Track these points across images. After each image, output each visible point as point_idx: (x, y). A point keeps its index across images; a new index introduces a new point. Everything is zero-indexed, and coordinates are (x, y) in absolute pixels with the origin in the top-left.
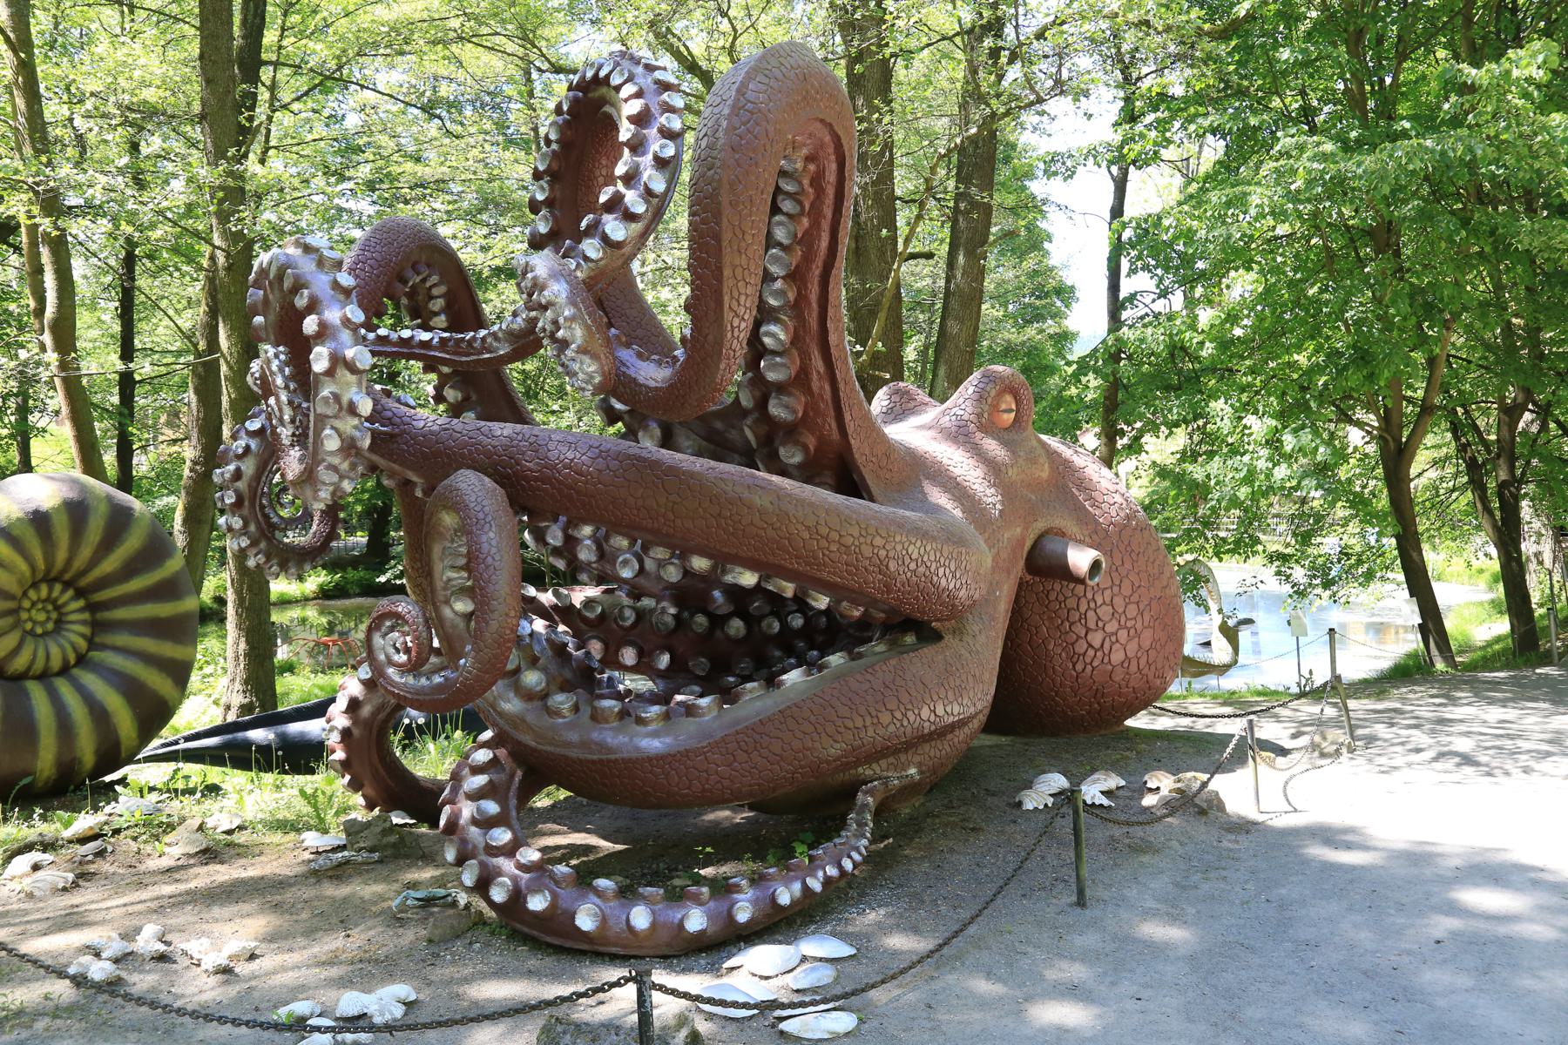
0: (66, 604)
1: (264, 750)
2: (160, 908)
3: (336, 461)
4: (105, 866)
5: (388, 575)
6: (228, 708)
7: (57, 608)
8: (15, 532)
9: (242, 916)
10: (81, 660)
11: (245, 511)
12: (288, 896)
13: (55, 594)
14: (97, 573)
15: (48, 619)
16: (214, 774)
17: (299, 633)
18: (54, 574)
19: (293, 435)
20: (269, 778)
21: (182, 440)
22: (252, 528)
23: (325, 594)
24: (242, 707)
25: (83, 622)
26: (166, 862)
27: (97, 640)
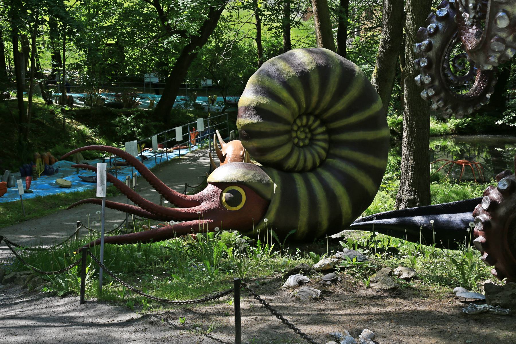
0: (316, 129)
1: (427, 230)
2: (370, 321)
3: (504, 35)
4: (337, 289)
5: (504, 119)
6: (400, 200)
7: (311, 131)
8: (292, 84)
9: (420, 335)
10: (323, 163)
11: (433, 72)
12: (448, 327)
13: (310, 122)
14: (333, 111)
15: (306, 137)
16: (394, 242)
17: (440, 156)
18: (310, 110)
19: (474, 17)
20: (429, 249)
21: (375, 28)
22: (437, 83)
23: (458, 131)
24: (409, 201)
25: (324, 141)
26: (370, 293)
27: (332, 152)
